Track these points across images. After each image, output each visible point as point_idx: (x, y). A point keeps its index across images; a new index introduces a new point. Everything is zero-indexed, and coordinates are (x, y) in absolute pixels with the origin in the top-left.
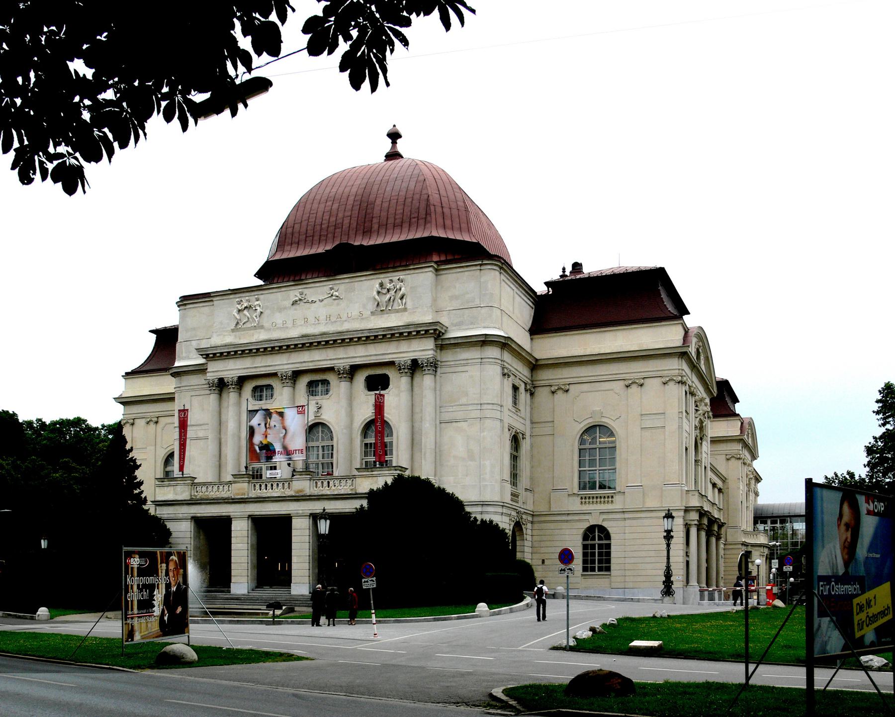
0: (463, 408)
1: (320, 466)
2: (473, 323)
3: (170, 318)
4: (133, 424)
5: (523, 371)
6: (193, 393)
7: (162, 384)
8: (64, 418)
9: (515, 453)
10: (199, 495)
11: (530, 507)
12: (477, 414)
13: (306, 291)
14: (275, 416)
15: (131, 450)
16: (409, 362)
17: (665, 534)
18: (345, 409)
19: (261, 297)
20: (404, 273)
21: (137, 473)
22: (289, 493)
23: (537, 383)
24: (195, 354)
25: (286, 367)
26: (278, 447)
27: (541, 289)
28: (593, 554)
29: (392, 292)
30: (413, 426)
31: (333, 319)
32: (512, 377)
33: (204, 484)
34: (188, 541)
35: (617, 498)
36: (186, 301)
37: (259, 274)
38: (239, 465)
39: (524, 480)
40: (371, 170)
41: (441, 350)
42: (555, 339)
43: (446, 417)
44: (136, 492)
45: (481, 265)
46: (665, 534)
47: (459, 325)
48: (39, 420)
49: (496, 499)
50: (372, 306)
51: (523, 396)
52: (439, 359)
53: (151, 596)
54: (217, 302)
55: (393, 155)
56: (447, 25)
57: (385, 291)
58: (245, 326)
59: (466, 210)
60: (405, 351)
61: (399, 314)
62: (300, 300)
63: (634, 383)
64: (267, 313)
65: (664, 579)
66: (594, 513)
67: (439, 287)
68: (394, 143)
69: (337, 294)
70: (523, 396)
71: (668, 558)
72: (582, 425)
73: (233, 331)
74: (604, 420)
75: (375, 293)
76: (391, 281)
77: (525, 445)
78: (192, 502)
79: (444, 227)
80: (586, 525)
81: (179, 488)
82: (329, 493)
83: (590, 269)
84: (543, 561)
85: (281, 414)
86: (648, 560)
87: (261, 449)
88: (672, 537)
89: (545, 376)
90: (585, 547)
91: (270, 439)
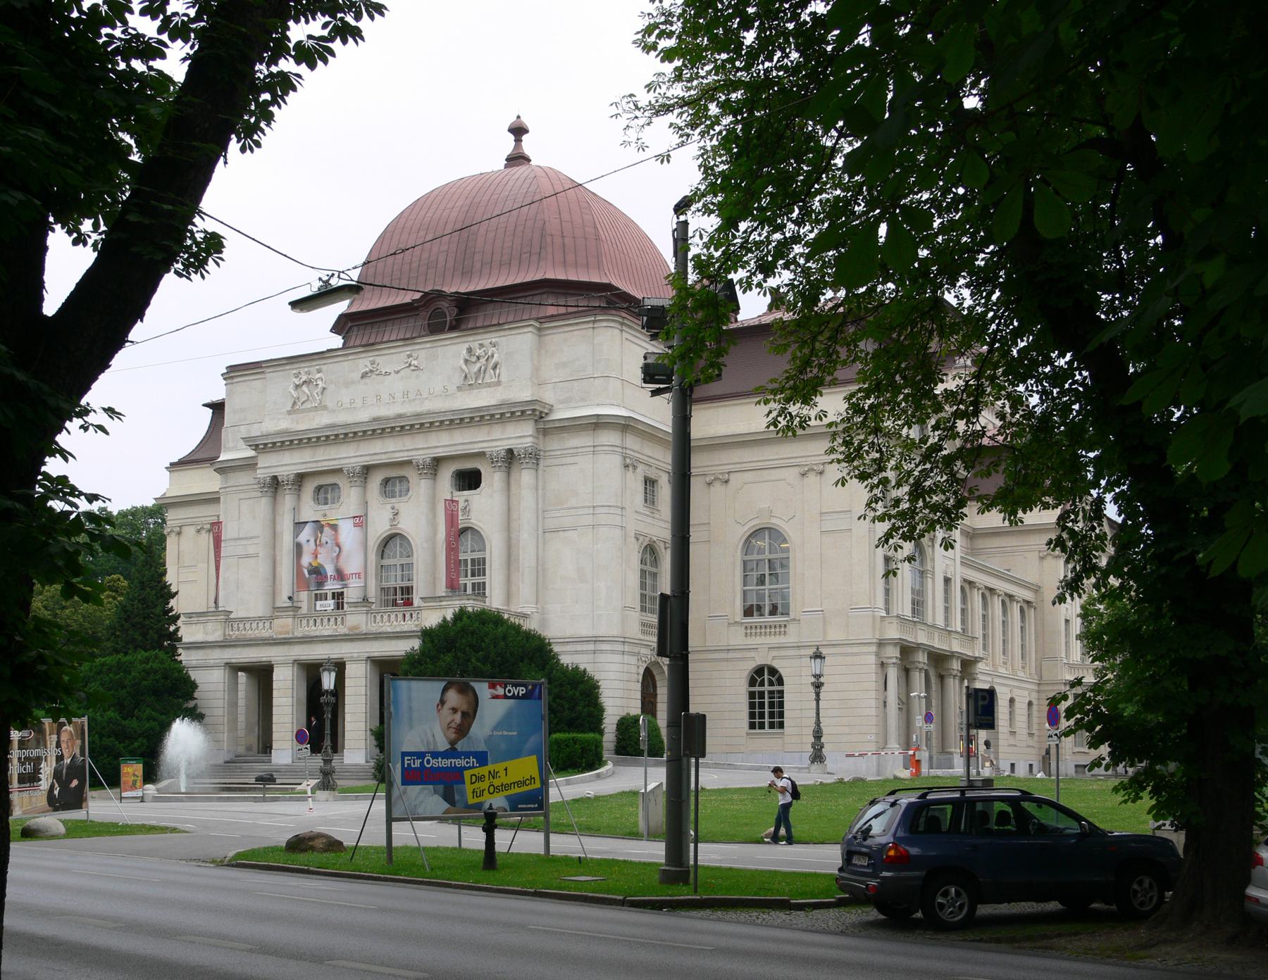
0: (573, 512)
1: (398, 591)
3: (218, 391)
4: (179, 533)
6: (243, 496)
8: (139, 505)
9: (648, 568)
10: (235, 634)
12: (588, 520)
13: (378, 360)
14: (327, 529)
16: (503, 453)
17: (813, 680)
18: (418, 515)
19: (324, 367)
21: (172, 603)
22: (342, 630)
24: (242, 444)
26: (330, 570)
28: (762, 705)
29: (483, 360)
31: (411, 396)
32: (641, 468)
33: (241, 620)
34: (220, 695)
35: (792, 628)
36: (234, 372)
38: (274, 594)
40: (478, 186)
42: (711, 411)
43: (551, 524)
44: (172, 628)
45: (594, 322)
46: (813, 680)
47: (567, 401)
49: (615, 633)
50: (458, 380)
53: (37, 771)
54: (270, 375)
55: (517, 159)
56: (203, 277)
58: (305, 406)
59: (598, 238)
62: (371, 371)
64: (331, 388)
65: (813, 740)
67: (543, 352)
68: (518, 140)
71: (818, 714)
73: (289, 413)
74: (774, 521)
75: (462, 362)
76: (481, 346)
78: (224, 644)
79: (565, 264)
80: (752, 665)
81: (210, 626)
82: (389, 630)
85: (334, 527)
87: (310, 573)
88: (822, 684)
90: (752, 695)
91: (320, 560)
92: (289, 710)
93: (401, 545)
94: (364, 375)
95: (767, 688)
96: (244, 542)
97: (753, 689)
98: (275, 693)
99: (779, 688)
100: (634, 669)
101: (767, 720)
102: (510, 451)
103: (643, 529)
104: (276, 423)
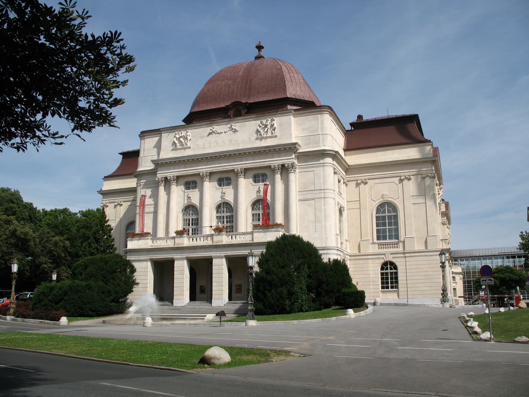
7: (130, 183)
15: (108, 220)
17: (441, 264)
28: (387, 279)
37: (184, 121)
46: (441, 264)
48: (43, 210)
60: (276, 161)
66: (388, 254)
72: (377, 202)
77: (345, 213)
80: (382, 261)
83: (365, 118)
86: (421, 281)
90: (382, 274)
95: (389, 271)
98: (175, 273)
101: (390, 285)
102: (283, 166)
104: (167, 154)
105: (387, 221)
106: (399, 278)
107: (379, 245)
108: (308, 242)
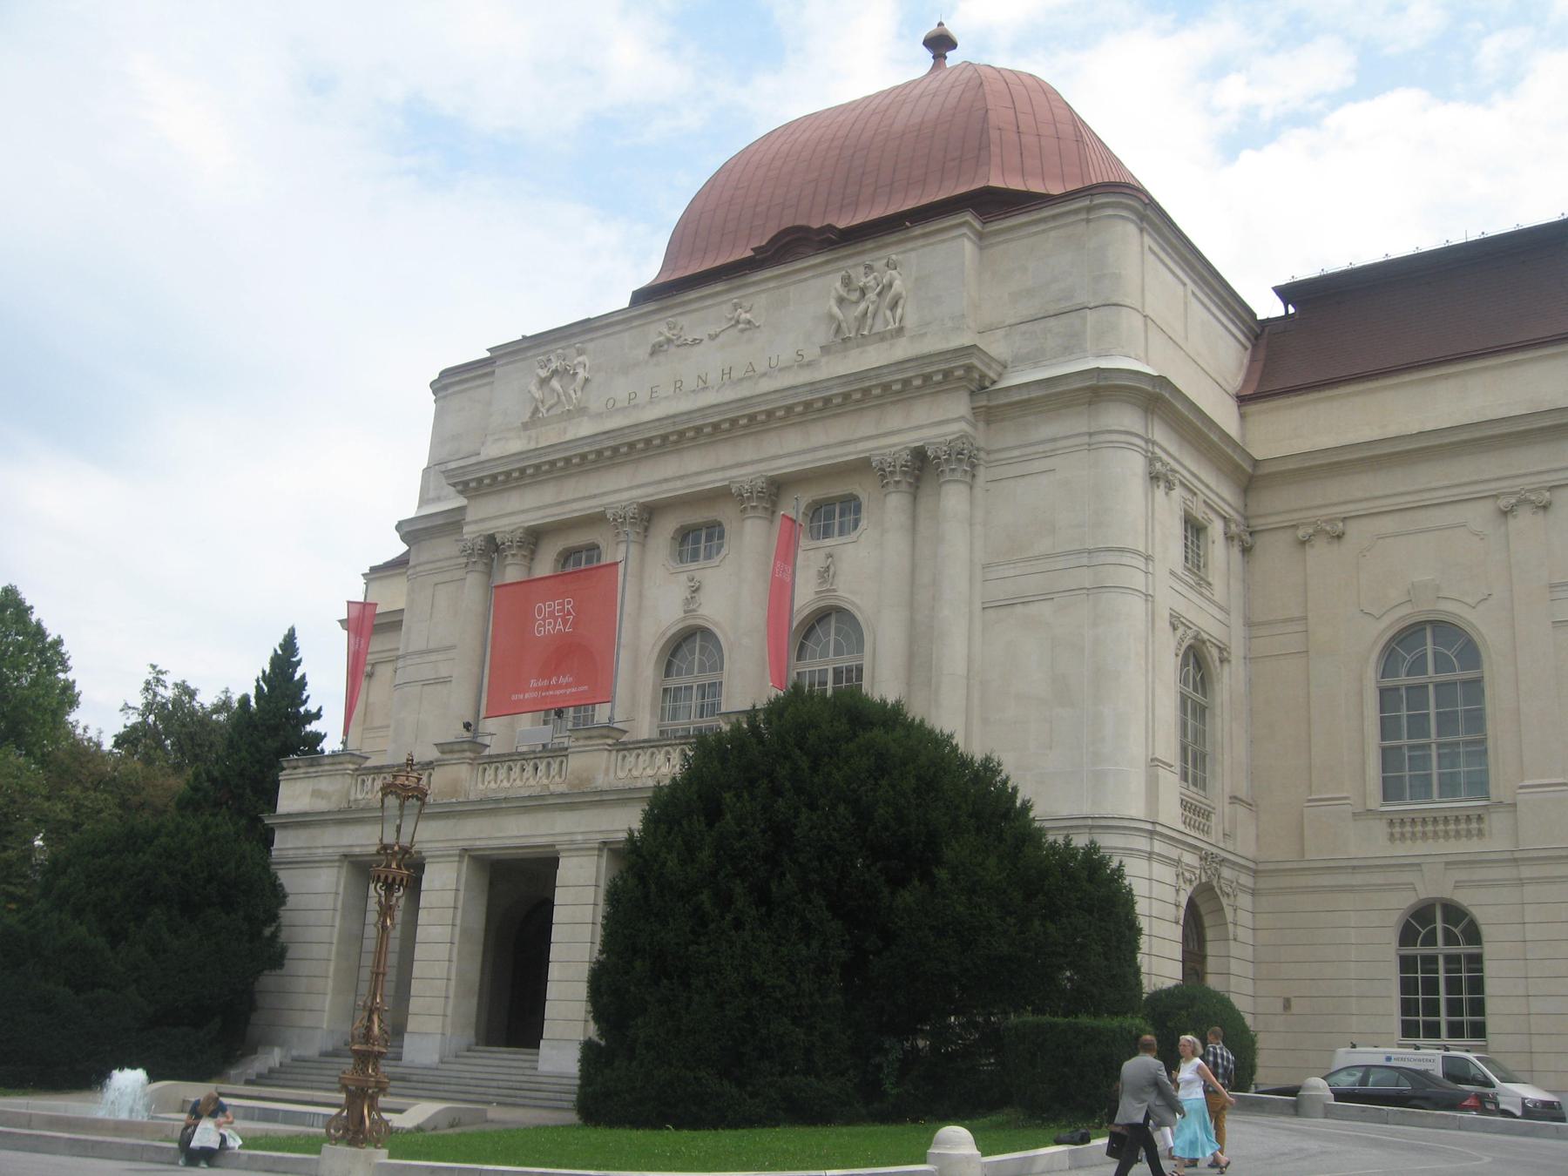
2: (1071, 348)
5: (1220, 492)
11: (1245, 846)
13: (683, 321)
16: (905, 456)
19: (590, 346)
20: (901, 248)
23: (1258, 523)
25: (626, 495)
27: (1269, 307)
28: (1431, 985)
29: (872, 296)
30: (912, 622)
35: (1497, 822)
39: (1229, 771)
41: (988, 423)
45: (1089, 209)
50: (823, 335)
51: (1218, 551)
52: (981, 442)
57: (855, 296)
61: (885, 345)
62: (669, 341)
63: (1522, 502)
69: (748, 316)
70: (1218, 551)
73: (525, 426)
75: (833, 303)
77: (1229, 682)
80: (1401, 903)
84: (1287, 1004)
89: (1277, 504)
90: (1406, 963)
92: (442, 951)
93: (703, 649)
94: (656, 350)
95: (1441, 949)
96: (433, 657)
97: (1409, 951)
99: (1472, 949)
100: (1169, 894)
101: (1443, 1019)
103: (1181, 607)
105: (1432, 711)
106: (1490, 987)
107: (1391, 823)
108: (989, 769)
